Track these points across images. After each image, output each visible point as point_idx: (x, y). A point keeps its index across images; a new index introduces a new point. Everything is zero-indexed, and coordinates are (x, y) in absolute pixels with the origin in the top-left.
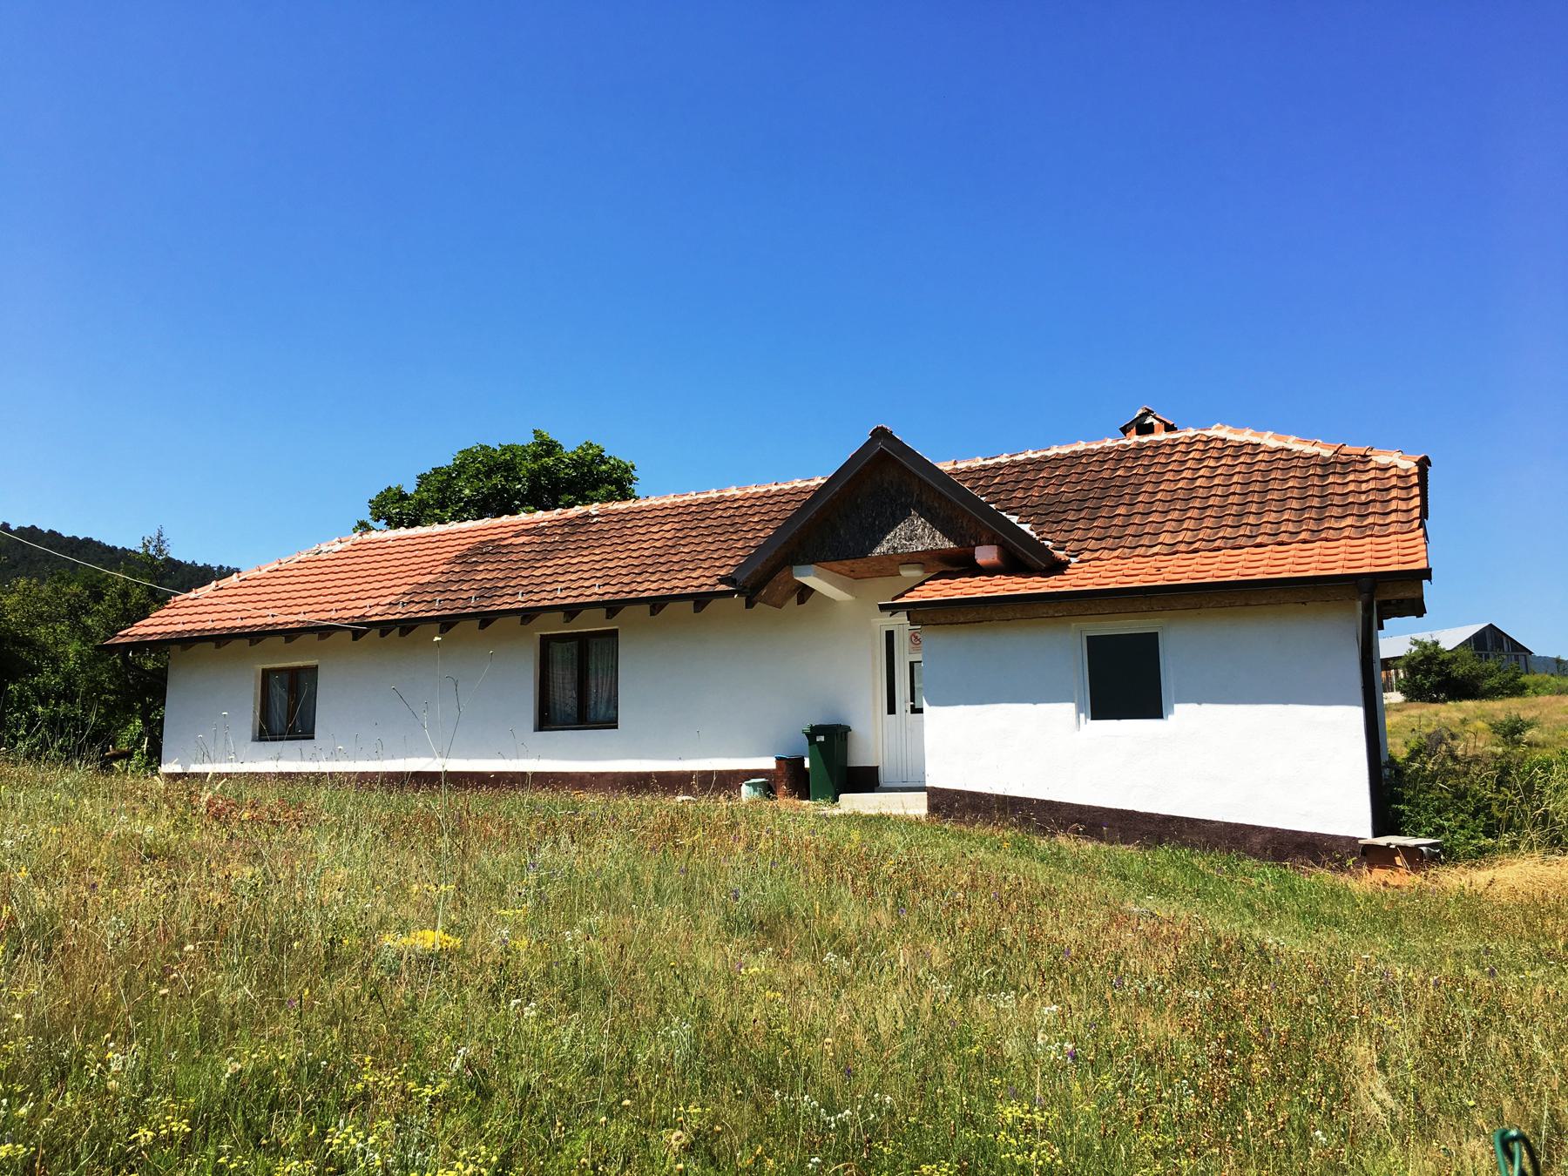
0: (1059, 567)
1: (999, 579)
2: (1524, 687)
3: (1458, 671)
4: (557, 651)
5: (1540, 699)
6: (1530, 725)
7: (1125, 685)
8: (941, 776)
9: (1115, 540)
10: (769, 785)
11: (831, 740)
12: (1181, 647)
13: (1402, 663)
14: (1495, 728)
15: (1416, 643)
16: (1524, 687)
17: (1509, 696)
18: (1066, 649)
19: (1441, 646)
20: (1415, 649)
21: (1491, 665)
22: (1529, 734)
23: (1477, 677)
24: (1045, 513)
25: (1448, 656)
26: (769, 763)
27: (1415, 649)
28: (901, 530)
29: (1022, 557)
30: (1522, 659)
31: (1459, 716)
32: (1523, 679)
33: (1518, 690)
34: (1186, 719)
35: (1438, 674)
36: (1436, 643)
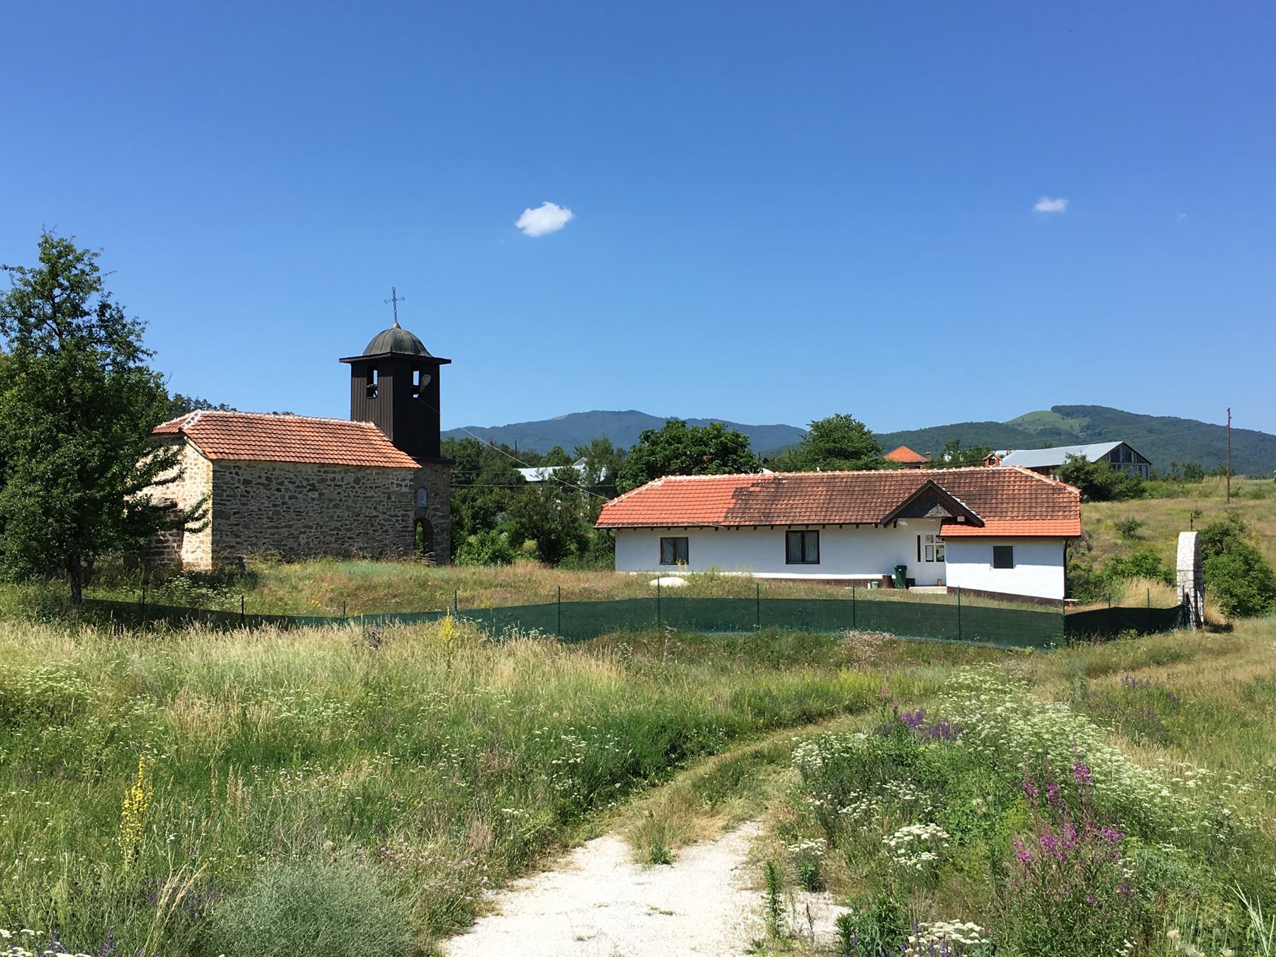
0: (982, 525)
1: (965, 527)
2: (1144, 491)
3: (1098, 479)
4: (792, 537)
5: (1154, 502)
6: (1140, 525)
7: (1003, 559)
8: (949, 584)
9: (1001, 515)
10: (880, 583)
11: (901, 570)
12: (1018, 550)
13: (1059, 471)
14: (1118, 527)
15: (1070, 457)
16: (1144, 491)
17: (1132, 498)
18: (988, 549)
19: (1088, 459)
20: (1069, 461)
21: (1122, 474)
22: (1139, 531)
23: (1113, 484)
24: (968, 497)
25: (1091, 468)
26: (880, 576)
27: (1069, 461)
28: (934, 509)
29: (972, 521)
30: (1144, 469)
31: (1096, 516)
32: (1145, 484)
33: (1138, 493)
34: (1020, 569)
35: (1084, 481)
36: (1084, 458)
